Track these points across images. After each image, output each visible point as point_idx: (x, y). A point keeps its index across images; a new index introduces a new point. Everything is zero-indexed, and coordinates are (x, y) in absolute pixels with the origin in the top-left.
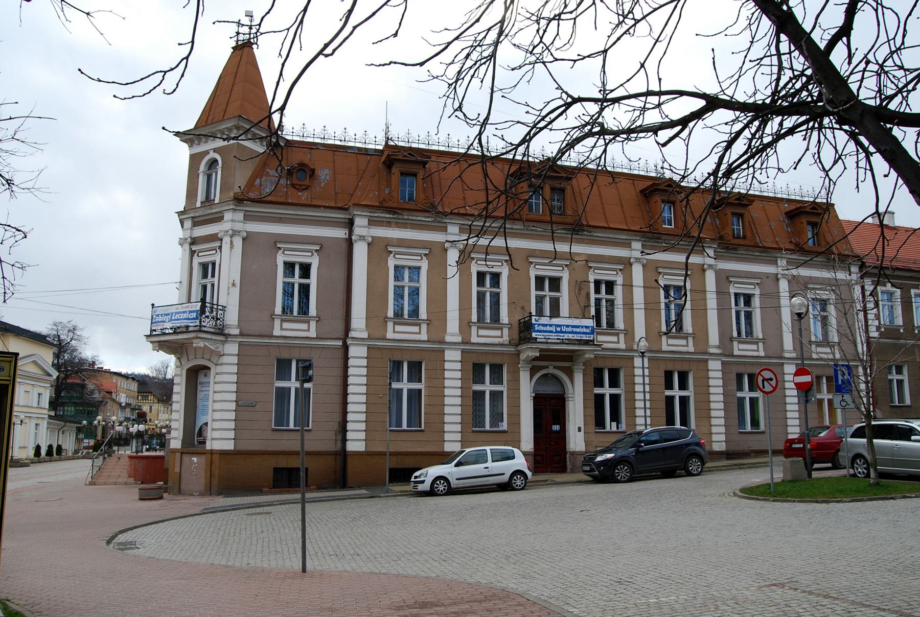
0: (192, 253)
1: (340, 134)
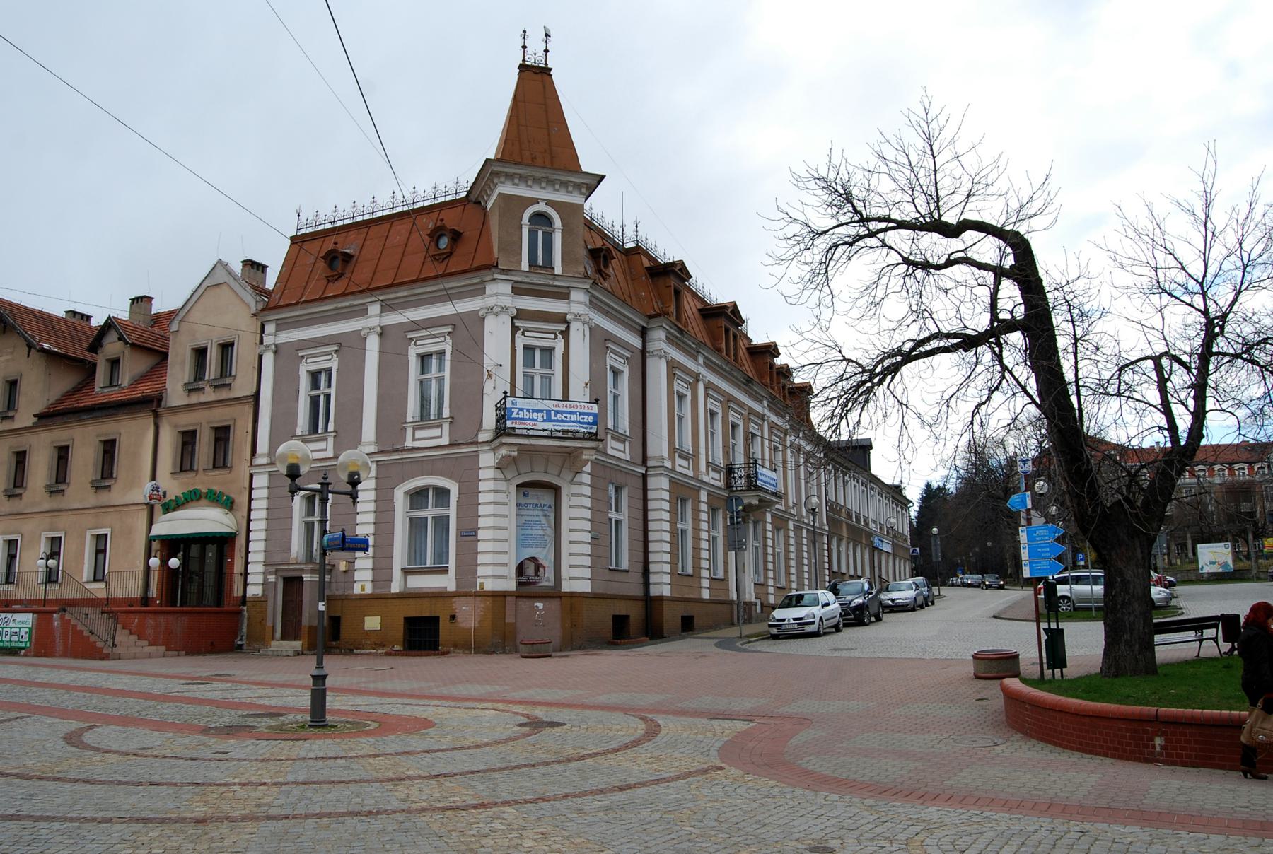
0: (515, 329)
1: (430, 194)
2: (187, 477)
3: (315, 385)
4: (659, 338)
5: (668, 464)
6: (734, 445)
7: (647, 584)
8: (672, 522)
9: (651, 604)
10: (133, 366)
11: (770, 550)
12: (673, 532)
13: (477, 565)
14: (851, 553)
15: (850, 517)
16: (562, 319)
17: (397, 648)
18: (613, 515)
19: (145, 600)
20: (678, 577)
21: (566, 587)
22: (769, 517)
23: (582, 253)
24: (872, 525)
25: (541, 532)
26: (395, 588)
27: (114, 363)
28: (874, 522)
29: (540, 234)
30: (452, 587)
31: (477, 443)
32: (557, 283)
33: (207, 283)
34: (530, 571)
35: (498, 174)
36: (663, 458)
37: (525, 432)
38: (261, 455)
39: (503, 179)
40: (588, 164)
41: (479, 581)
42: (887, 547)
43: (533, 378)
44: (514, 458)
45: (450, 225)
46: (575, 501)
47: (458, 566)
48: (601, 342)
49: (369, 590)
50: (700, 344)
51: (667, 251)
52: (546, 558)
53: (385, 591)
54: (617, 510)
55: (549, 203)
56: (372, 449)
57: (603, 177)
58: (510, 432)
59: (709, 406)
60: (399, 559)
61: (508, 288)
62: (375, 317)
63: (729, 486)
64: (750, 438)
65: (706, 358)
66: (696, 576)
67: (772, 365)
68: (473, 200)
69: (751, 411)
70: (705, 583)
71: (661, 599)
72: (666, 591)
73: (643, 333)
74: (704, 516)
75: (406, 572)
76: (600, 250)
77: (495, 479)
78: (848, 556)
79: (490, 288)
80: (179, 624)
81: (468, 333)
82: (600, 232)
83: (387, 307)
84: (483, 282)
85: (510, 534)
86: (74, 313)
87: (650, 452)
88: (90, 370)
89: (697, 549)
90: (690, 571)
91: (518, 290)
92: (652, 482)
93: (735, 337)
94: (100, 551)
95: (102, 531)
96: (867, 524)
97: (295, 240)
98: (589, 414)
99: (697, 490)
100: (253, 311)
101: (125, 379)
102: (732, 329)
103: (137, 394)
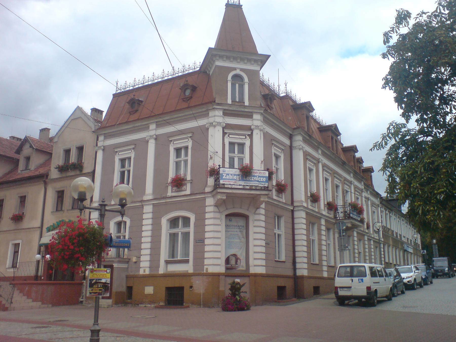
0: (224, 134)
2: (59, 214)
3: (123, 166)
4: (298, 140)
5: (305, 205)
6: (337, 196)
7: (295, 269)
8: (308, 235)
9: (297, 280)
10: (37, 161)
11: (356, 251)
12: (308, 241)
13: (204, 258)
14: (394, 253)
15: (393, 235)
16: (249, 128)
17: (162, 304)
18: (277, 231)
19: (36, 277)
20: (311, 265)
21: (253, 270)
22: (355, 234)
23: (259, 96)
24: (403, 239)
25: (238, 240)
26: (161, 271)
27: (28, 159)
28: (404, 237)
29: (237, 85)
30: (191, 271)
31: (204, 193)
32: (246, 110)
33: (72, 118)
34: (233, 262)
35: (215, 55)
36: (302, 201)
37: (230, 186)
38: (95, 202)
39: (218, 58)
40: (261, 50)
41: (205, 267)
42: (411, 250)
43: (234, 159)
44: (224, 200)
45: (191, 83)
46: (257, 223)
47: (195, 259)
48: (269, 141)
49: (147, 272)
50: (319, 143)
51: (301, 97)
52: (241, 255)
53: (155, 273)
54: (278, 229)
55: (242, 70)
56: (151, 197)
57: (268, 56)
58: (223, 187)
59: (324, 176)
60: (164, 255)
61: (221, 113)
62: (153, 130)
63: (335, 217)
64: (345, 193)
65: (322, 151)
66: (320, 265)
67: (354, 157)
68: (204, 71)
69: (345, 179)
70: (325, 268)
71: (302, 277)
72: (305, 273)
73: (291, 137)
74: (323, 233)
75: (167, 262)
76: (267, 95)
77: (214, 212)
78: (392, 254)
79: (211, 114)
80: (50, 290)
81: (201, 137)
82: (267, 87)
83: (159, 126)
84: (208, 110)
85: (222, 241)
86: (14, 138)
87: (295, 199)
88: (16, 162)
89: (320, 250)
90: (317, 262)
91: (226, 113)
92: (296, 214)
93: (336, 141)
94: (16, 252)
95: (17, 242)
96: (401, 238)
97: (114, 95)
98: (263, 177)
99: (320, 218)
100: (93, 130)
101: (33, 166)
102: (335, 137)
103: (37, 173)
